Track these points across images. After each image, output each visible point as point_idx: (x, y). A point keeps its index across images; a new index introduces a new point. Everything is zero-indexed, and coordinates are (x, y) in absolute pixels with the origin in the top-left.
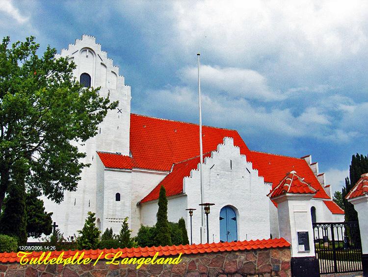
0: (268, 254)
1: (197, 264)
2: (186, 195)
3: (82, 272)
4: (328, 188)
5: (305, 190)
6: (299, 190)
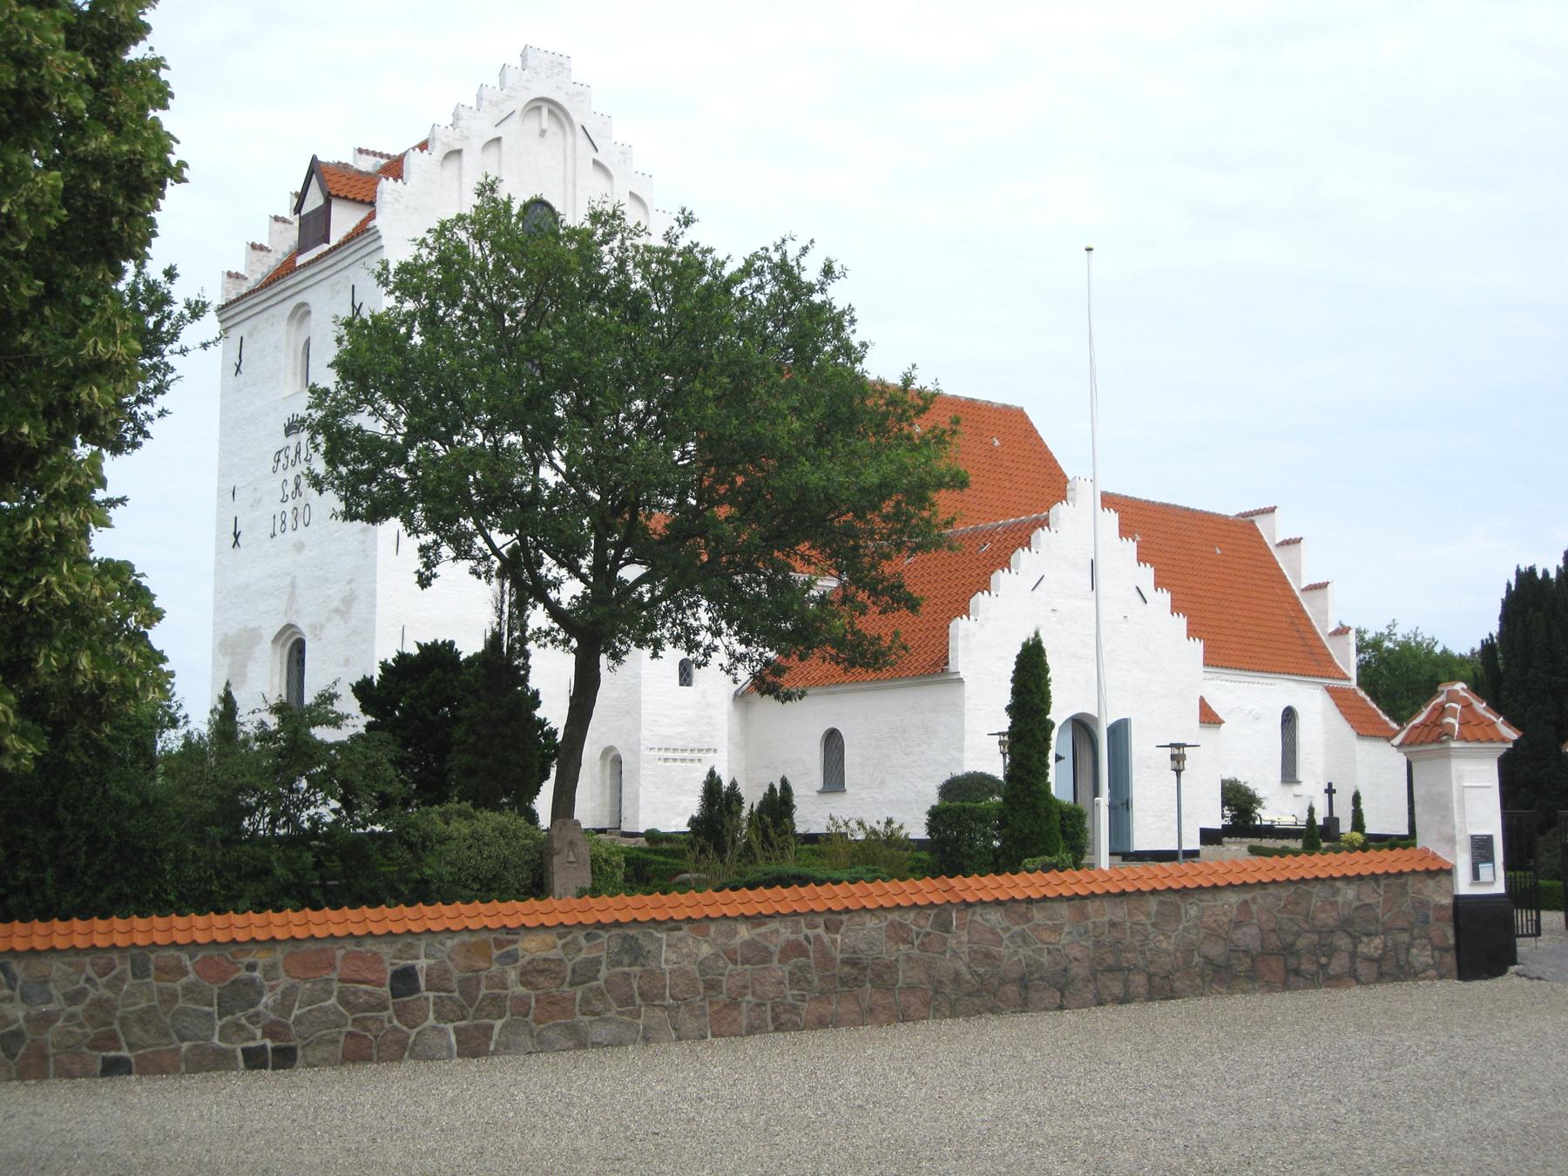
0: (1404, 886)
1: (1254, 908)
2: (961, 681)
3: (1008, 929)
4: (1339, 639)
5: (1492, 735)
6: (1479, 733)
